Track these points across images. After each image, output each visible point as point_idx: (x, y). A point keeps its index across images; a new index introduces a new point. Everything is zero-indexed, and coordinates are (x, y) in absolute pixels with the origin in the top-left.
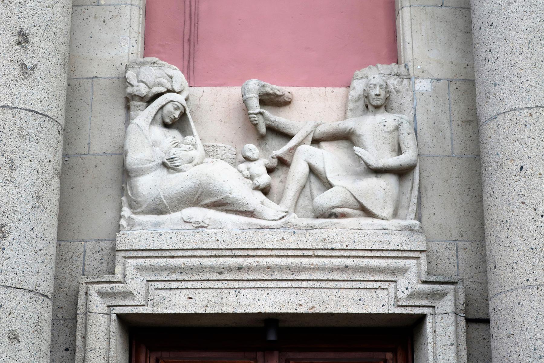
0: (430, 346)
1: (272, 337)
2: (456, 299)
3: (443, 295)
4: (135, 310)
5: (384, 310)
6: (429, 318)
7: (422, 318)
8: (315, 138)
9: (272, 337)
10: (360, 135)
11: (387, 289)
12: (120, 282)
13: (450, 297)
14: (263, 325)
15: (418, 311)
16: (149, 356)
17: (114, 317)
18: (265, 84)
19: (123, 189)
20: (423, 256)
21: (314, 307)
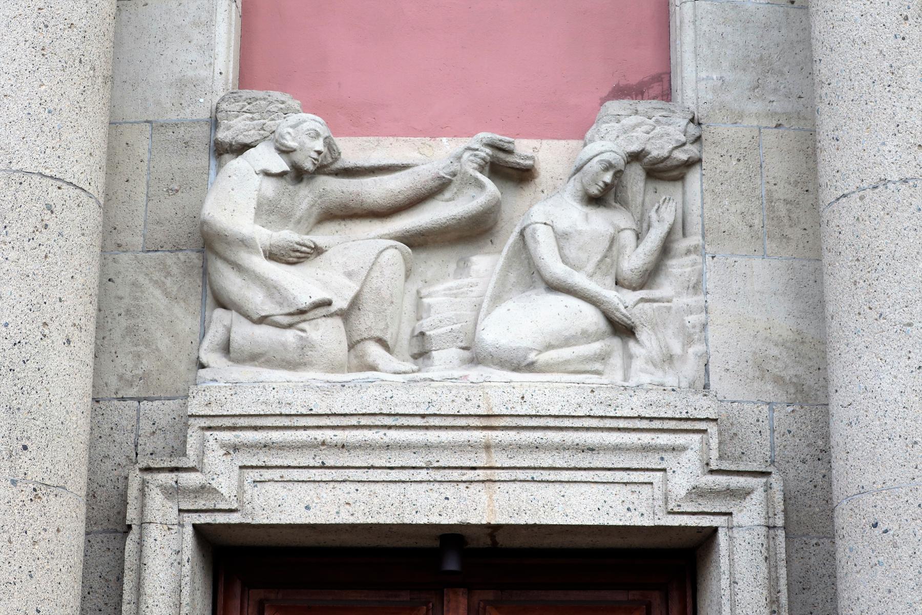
0: (724, 582)
1: (452, 564)
2: (769, 501)
3: (745, 493)
4: (221, 519)
5: (647, 522)
6: (722, 536)
7: (713, 531)
8: (679, 184)
9: (452, 564)
10: (538, 241)
11: (652, 483)
12: (193, 469)
13: (758, 496)
14: (437, 544)
15: (705, 522)
16: (246, 605)
17: (189, 531)
18: (307, 234)
19: (614, 237)
20: (712, 428)
21: (376, 433)
